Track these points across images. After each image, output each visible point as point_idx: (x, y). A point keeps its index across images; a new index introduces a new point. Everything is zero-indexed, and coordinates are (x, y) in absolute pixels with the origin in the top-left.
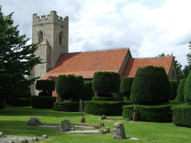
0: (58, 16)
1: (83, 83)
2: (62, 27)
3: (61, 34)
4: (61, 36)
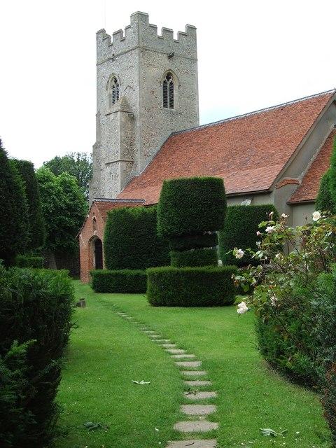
0: (154, 27)
1: (223, 204)
2: (170, 57)
3: (168, 78)
4: (169, 83)
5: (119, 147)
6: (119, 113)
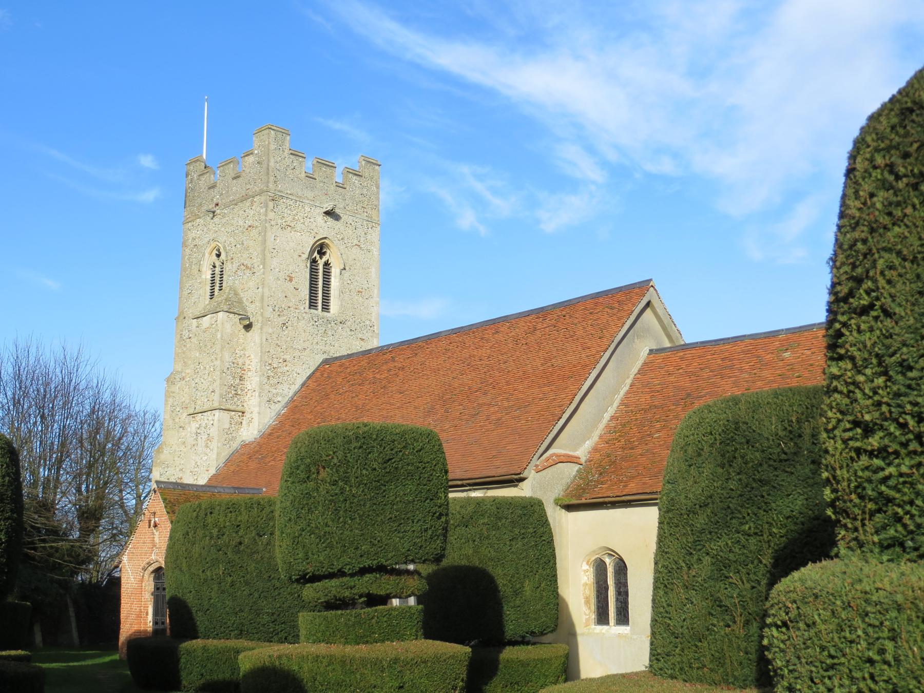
5: (218, 382)
6: (220, 314)
